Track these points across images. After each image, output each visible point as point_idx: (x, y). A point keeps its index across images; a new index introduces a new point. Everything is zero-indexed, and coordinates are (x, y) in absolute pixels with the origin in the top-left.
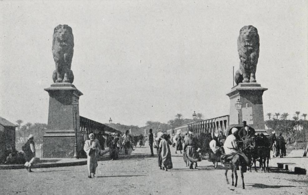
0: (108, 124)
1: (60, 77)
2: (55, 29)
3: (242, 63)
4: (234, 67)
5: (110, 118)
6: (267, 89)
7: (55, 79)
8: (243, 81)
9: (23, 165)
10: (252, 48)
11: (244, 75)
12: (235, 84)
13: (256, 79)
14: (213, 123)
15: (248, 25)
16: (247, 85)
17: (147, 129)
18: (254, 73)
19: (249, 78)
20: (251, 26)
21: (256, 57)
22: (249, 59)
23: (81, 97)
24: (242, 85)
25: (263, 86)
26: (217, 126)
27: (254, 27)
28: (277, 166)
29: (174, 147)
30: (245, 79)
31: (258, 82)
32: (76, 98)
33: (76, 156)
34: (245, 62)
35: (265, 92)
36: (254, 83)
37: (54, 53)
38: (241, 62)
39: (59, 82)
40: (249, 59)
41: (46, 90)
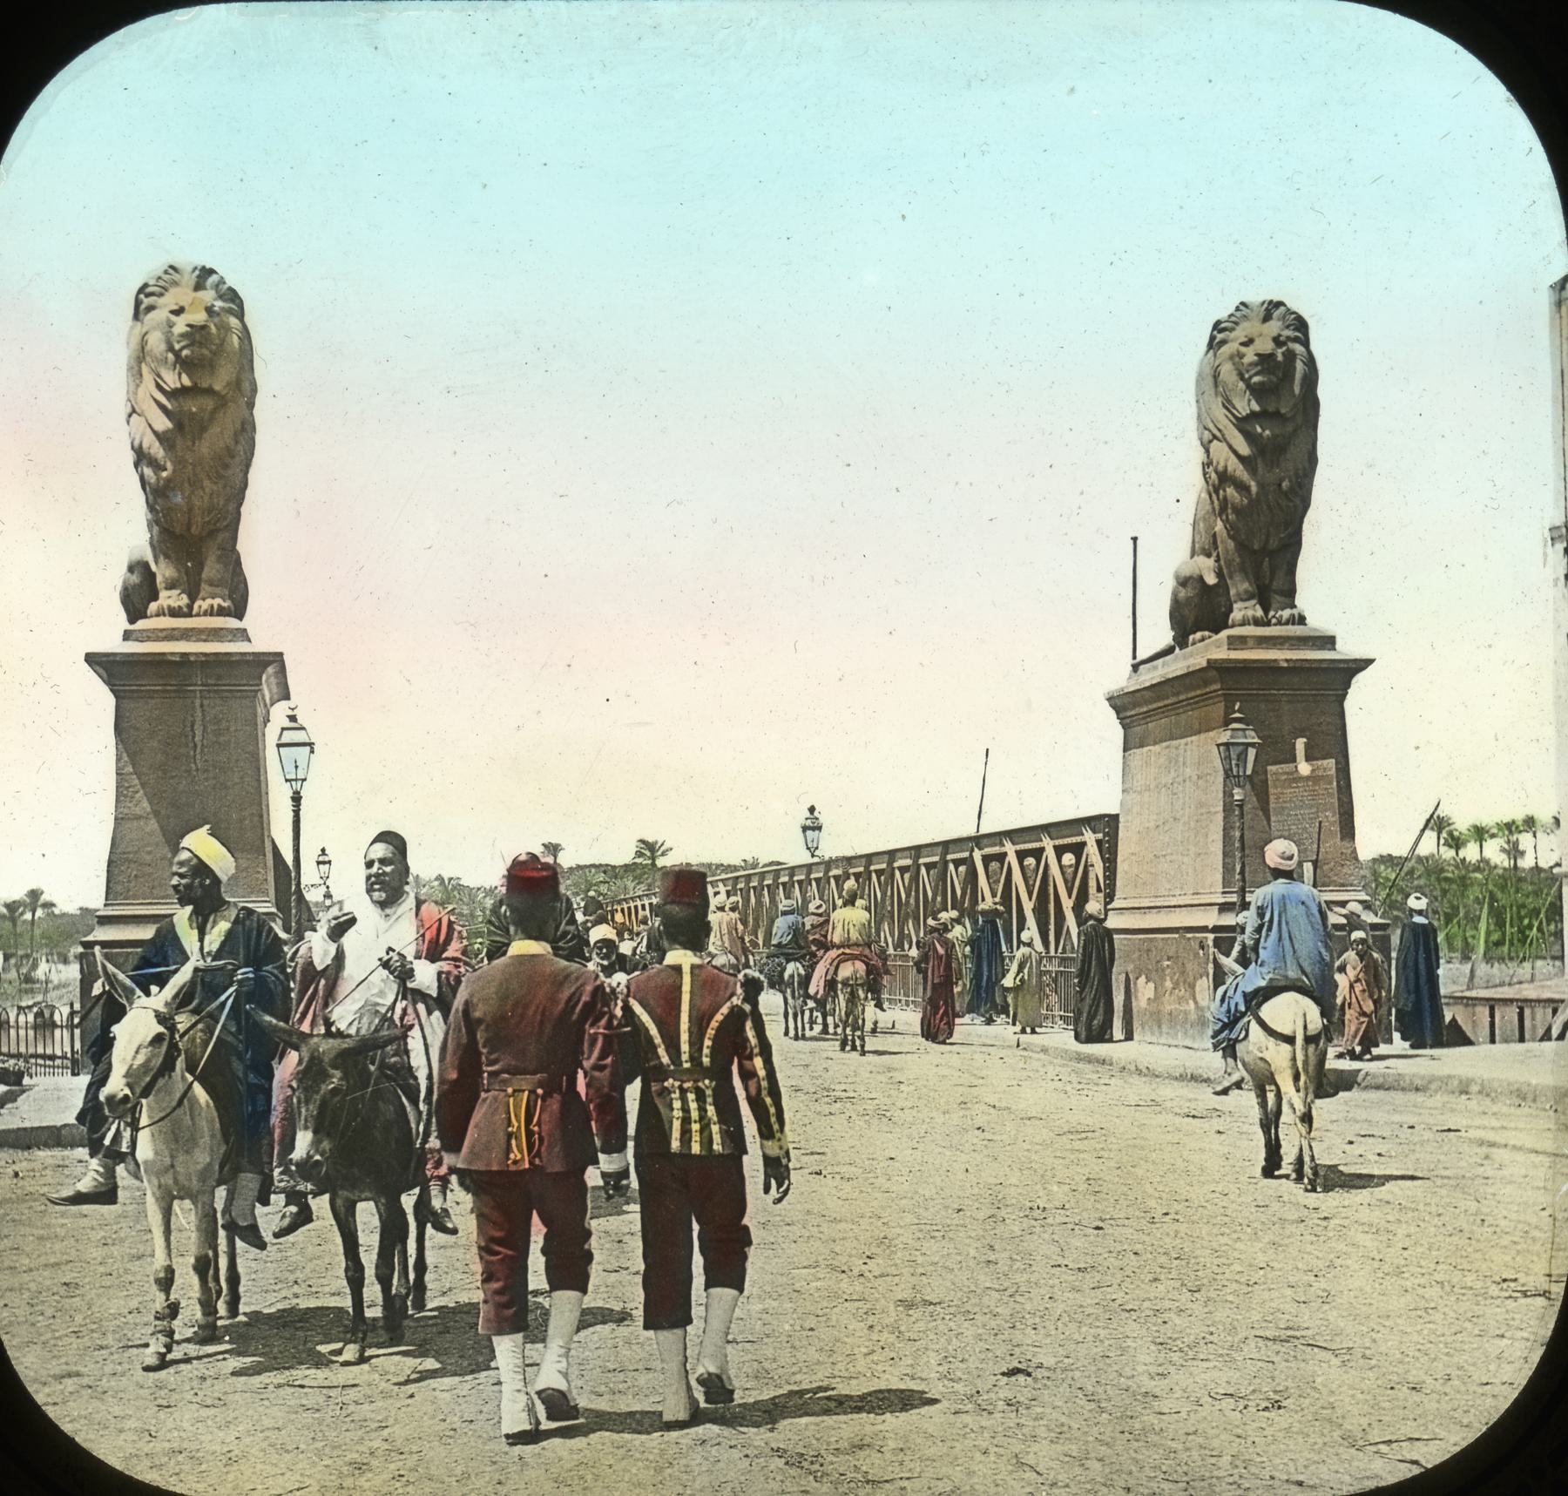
2: (1217, 326)
4: (1135, 539)
5: (812, 810)
7: (137, 598)
15: (1261, 299)
20: (1280, 304)
23: (1360, 700)
24: (1236, 642)
25: (1347, 648)
27: (1289, 312)
31: (1318, 621)
33: (163, 1009)
35: (1360, 681)
39: (175, 613)
41: (92, 659)
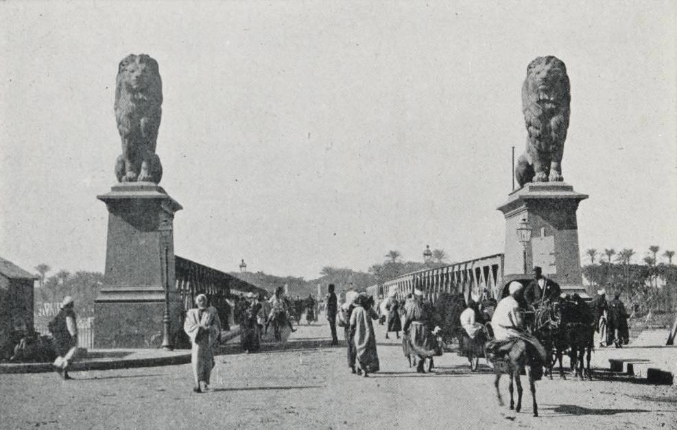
0: (237, 274)
1: (132, 170)
2: (121, 64)
3: (533, 139)
4: (513, 148)
5: (243, 261)
6: (587, 197)
7: (121, 174)
8: (535, 178)
9: (51, 365)
10: (554, 106)
11: (537, 166)
12: (517, 185)
13: (563, 175)
14: (468, 271)
15: (545, 56)
16: (543, 188)
17: (323, 285)
18: (559, 161)
19: (548, 173)
20: (552, 57)
21: (563, 126)
22: (546, 130)
23: (177, 214)
24: (532, 188)
25: (578, 190)
26: (478, 277)
27: (557, 60)
28: (608, 366)
29: (383, 324)
30: (539, 175)
31: (567, 181)
32: (166, 217)
34: (539, 138)
35: (582, 203)
36: (559, 184)
37: (119, 116)
38: (530, 136)
39: (131, 180)
40: (546, 130)
41: (102, 199)
